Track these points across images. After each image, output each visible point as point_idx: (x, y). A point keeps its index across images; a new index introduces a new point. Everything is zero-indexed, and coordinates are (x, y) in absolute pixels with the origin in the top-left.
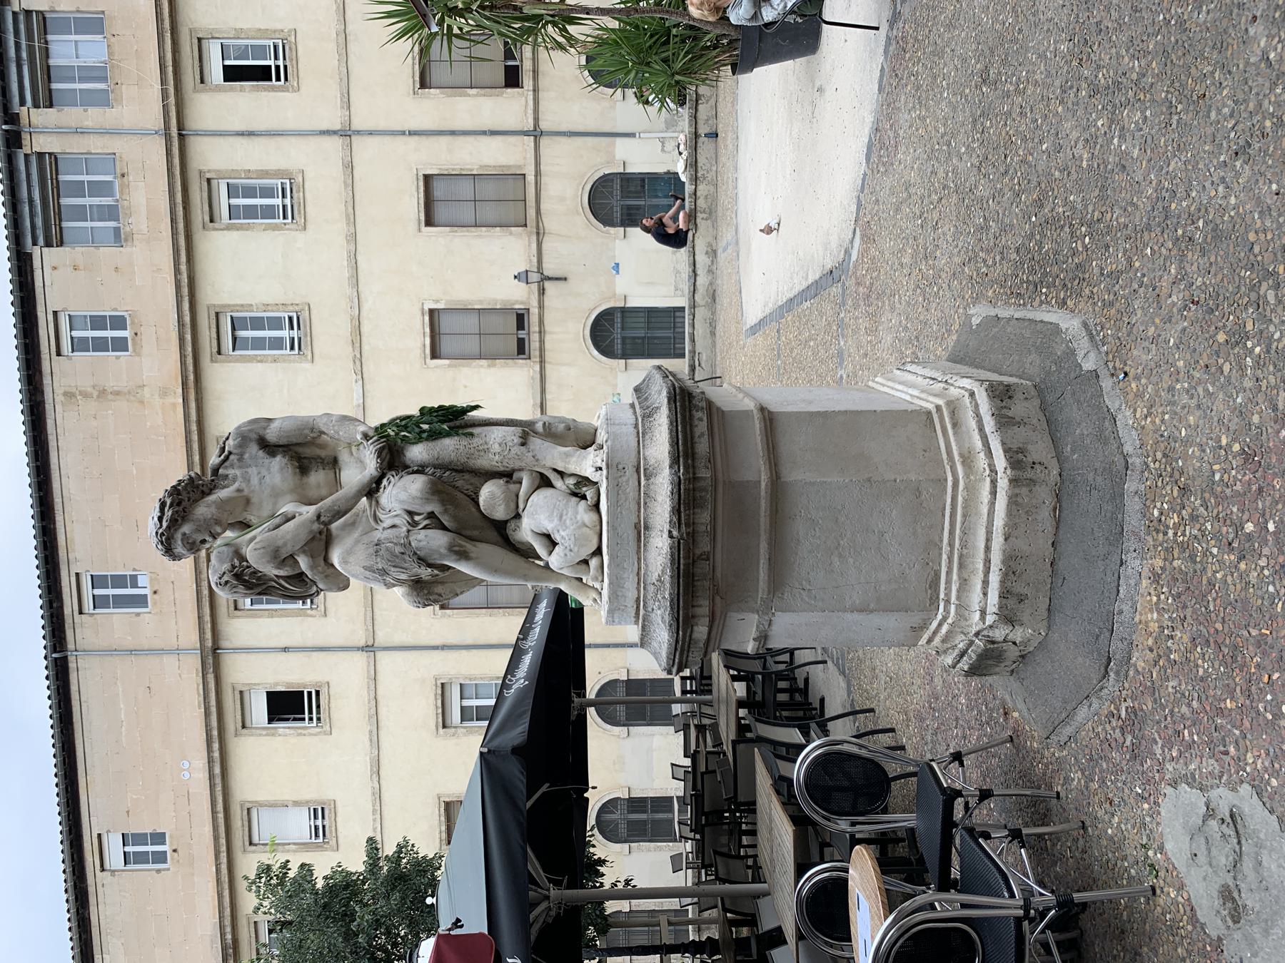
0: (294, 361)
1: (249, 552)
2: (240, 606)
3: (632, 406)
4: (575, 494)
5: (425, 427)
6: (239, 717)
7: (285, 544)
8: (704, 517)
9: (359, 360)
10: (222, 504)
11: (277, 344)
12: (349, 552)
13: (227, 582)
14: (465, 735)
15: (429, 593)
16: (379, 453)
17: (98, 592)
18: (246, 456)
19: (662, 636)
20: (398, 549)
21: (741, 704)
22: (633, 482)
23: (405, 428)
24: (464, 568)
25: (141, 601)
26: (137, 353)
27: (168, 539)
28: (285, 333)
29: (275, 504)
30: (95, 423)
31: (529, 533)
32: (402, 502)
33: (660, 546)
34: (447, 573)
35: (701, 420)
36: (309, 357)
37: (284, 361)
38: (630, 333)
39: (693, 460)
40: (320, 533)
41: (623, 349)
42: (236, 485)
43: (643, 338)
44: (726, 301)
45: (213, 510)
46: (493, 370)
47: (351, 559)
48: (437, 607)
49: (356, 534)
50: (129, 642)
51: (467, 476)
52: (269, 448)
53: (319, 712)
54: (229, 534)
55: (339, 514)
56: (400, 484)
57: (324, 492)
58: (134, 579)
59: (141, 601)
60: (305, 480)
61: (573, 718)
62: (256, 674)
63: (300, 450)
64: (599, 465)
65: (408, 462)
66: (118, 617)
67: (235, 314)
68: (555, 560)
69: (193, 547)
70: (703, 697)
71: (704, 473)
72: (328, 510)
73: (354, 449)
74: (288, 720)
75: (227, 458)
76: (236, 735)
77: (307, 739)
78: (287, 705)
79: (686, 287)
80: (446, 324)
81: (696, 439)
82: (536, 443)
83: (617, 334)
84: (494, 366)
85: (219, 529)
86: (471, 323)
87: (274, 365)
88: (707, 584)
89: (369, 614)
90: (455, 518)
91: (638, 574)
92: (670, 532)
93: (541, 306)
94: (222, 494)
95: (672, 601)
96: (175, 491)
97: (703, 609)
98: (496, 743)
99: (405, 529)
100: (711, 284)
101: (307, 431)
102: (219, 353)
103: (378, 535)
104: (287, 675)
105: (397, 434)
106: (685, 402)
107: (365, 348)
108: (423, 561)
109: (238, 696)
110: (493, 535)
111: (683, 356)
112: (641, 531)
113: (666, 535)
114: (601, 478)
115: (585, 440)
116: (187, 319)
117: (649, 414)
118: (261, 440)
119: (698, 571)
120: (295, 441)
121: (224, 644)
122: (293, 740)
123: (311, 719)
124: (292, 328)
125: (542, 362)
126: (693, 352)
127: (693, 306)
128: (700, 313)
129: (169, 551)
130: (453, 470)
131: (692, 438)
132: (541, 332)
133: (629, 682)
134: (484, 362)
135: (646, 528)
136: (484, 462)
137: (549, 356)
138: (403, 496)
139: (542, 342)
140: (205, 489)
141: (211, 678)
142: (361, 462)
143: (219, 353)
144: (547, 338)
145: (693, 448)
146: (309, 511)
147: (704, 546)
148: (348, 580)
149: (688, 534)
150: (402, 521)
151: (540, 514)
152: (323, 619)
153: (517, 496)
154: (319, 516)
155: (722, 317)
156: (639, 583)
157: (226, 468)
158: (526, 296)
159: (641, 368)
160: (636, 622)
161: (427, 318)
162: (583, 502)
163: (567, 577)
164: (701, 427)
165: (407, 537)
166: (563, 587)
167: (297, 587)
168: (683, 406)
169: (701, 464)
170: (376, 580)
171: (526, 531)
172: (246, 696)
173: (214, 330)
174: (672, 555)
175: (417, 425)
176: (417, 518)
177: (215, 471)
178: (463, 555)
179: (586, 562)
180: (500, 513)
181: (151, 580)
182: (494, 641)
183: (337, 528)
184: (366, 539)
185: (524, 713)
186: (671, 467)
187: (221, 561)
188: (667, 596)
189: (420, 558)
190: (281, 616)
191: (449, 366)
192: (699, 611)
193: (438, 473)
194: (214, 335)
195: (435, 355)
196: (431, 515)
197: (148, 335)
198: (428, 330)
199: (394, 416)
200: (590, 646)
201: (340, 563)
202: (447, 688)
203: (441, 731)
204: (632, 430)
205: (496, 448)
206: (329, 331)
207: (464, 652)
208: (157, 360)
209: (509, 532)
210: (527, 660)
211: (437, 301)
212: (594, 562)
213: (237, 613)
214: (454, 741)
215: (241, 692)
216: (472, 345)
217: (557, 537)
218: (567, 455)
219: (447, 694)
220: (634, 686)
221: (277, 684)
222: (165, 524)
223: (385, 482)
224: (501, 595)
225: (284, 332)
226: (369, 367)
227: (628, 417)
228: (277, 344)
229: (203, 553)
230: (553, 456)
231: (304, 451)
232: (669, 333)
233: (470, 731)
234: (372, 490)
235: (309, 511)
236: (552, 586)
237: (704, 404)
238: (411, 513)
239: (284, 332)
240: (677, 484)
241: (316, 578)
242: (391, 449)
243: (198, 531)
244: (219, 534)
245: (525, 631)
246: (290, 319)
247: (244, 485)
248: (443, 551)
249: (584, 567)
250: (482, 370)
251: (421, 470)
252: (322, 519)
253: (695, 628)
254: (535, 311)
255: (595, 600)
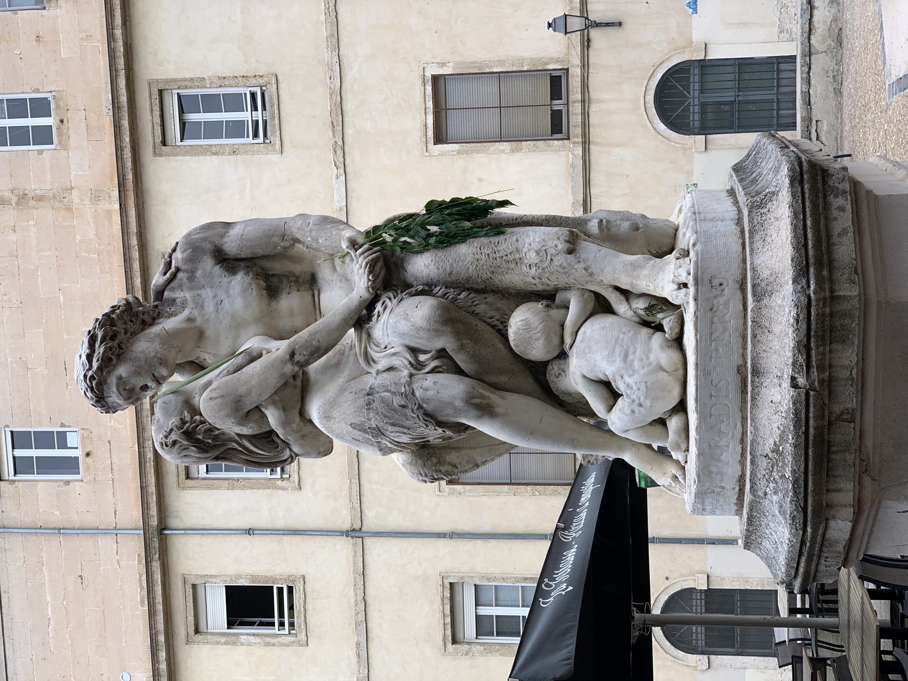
0: (258, 152)
1: (203, 402)
2: (193, 473)
3: (732, 192)
4: (646, 324)
5: (434, 229)
6: (191, 618)
7: (249, 392)
8: (847, 357)
9: (341, 148)
10: (170, 337)
11: (236, 129)
12: (332, 404)
13: (174, 443)
14: (481, 654)
15: (439, 463)
16: (372, 267)
17: (19, 453)
18: (199, 273)
19: (780, 533)
20: (397, 401)
21: (883, 632)
22: (735, 305)
23: (407, 231)
24: (487, 428)
25: (70, 465)
26: (64, 146)
27: (99, 384)
28: (246, 116)
29: (236, 338)
30: (13, 237)
31: (580, 380)
32: (402, 335)
33: (776, 402)
34: (464, 435)
35: (842, 209)
36: (278, 146)
37: (246, 152)
38: (710, 97)
39: (831, 271)
40: (294, 377)
41: (703, 120)
42: (186, 313)
43: (732, 103)
44: (858, 44)
45: (156, 345)
46: (518, 156)
47: (336, 414)
48: (443, 483)
49: (341, 380)
50: (56, 517)
51: (491, 298)
52: (228, 262)
53: (291, 616)
54: (177, 378)
55: (318, 352)
56: (398, 310)
57: (298, 321)
58: (62, 436)
59: (70, 465)
60: (274, 305)
61: (633, 641)
62: (214, 562)
63: (267, 264)
64: (683, 279)
65: (410, 279)
66: (43, 485)
67: (183, 92)
68: (617, 420)
69: (132, 395)
70: (820, 620)
71: (848, 290)
72: (304, 346)
73: (338, 262)
74: (252, 624)
75: (174, 276)
76: (188, 642)
77: (277, 650)
78: (252, 605)
79: (797, 28)
80: (455, 95)
81: (835, 239)
82: (590, 250)
83: (694, 98)
84: (519, 150)
85: (164, 372)
86: (488, 92)
87: (232, 158)
88: (850, 458)
89: (355, 488)
90: (474, 357)
91: (743, 441)
92: (793, 379)
93: (585, 65)
94: (169, 324)
95: (795, 482)
96: (107, 321)
97: (845, 493)
98: (530, 671)
99: (406, 373)
100: (835, 20)
101: (276, 239)
102: (164, 143)
103: (370, 381)
104: (254, 564)
105: (395, 240)
106: (816, 182)
107: (349, 131)
108: (431, 417)
109: (190, 591)
110: (528, 382)
111: (793, 126)
112: (748, 377)
113: (786, 383)
114: (687, 300)
115: (661, 244)
116: (124, 99)
117: (760, 203)
118: (218, 252)
119: (837, 437)
120: (260, 252)
121: (173, 522)
122: (259, 651)
123: (282, 624)
124: (255, 108)
125: (586, 143)
126: (808, 120)
127: (809, 53)
128: (819, 63)
129: (101, 400)
130: (471, 290)
131: (829, 237)
132: (585, 101)
133: (709, 592)
134: (505, 146)
135: (756, 372)
136: (515, 278)
137: (596, 134)
138: (404, 326)
139: (585, 114)
140: (146, 317)
141: (156, 566)
142: (347, 280)
143: (164, 143)
144: (594, 109)
145: (830, 252)
146: (280, 348)
147: (847, 400)
148: (331, 442)
149: (821, 382)
150: (402, 361)
151: (594, 353)
152: (297, 493)
153: (562, 326)
154: (292, 355)
155: (851, 67)
156: (743, 454)
157: (173, 289)
158: (564, 51)
159: (734, 146)
160: (739, 512)
161: (429, 88)
162: (658, 335)
163: (634, 444)
164: (843, 221)
165: (410, 384)
166: (628, 458)
167: (265, 451)
168: (814, 191)
169: (842, 276)
170: (367, 442)
171: (575, 376)
172: (200, 591)
173: (157, 113)
174: (796, 413)
175: (423, 225)
176: (422, 358)
177: (160, 294)
178: (486, 410)
179: (662, 422)
180: (537, 351)
181: (83, 438)
182: (520, 528)
183: (317, 371)
184: (354, 386)
185: (569, 629)
186: (795, 281)
187: (167, 413)
188: (788, 474)
189: (426, 414)
190: (244, 488)
191: (459, 152)
192: (838, 498)
193: (452, 293)
194: (157, 120)
195: (440, 138)
196: (442, 354)
197: (76, 121)
198: (430, 104)
199: (391, 215)
200: (654, 540)
201: (320, 418)
202: (458, 589)
203: (450, 647)
204: (733, 227)
205: (532, 257)
206: (302, 113)
207: (479, 543)
208: (86, 157)
209: (551, 378)
210: (571, 556)
211: (443, 65)
212: (674, 423)
213: (189, 482)
214: (466, 662)
215: (194, 586)
216: (490, 122)
217: (620, 385)
218: (635, 266)
219: (458, 598)
220: (716, 598)
221: (239, 577)
222: (95, 365)
223: (379, 307)
224: (528, 466)
225: (243, 113)
226: (354, 158)
227: (726, 208)
228: (236, 129)
229: (146, 402)
230: (615, 268)
231: (272, 266)
232: (770, 95)
233: (489, 649)
234: (362, 318)
235: (280, 348)
236: (612, 456)
237: (847, 186)
238: (414, 351)
239: (243, 113)
240: (805, 309)
241: (290, 439)
242: (388, 258)
243: (137, 373)
244: (165, 378)
245: (567, 517)
246: (253, 95)
247: (196, 312)
248: (459, 404)
249: (659, 429)
250: (504, 156)
251: (427, 290)
252: (297, 358)
253: (832, 523)
254: (576, 72)
255: (675, 478)
